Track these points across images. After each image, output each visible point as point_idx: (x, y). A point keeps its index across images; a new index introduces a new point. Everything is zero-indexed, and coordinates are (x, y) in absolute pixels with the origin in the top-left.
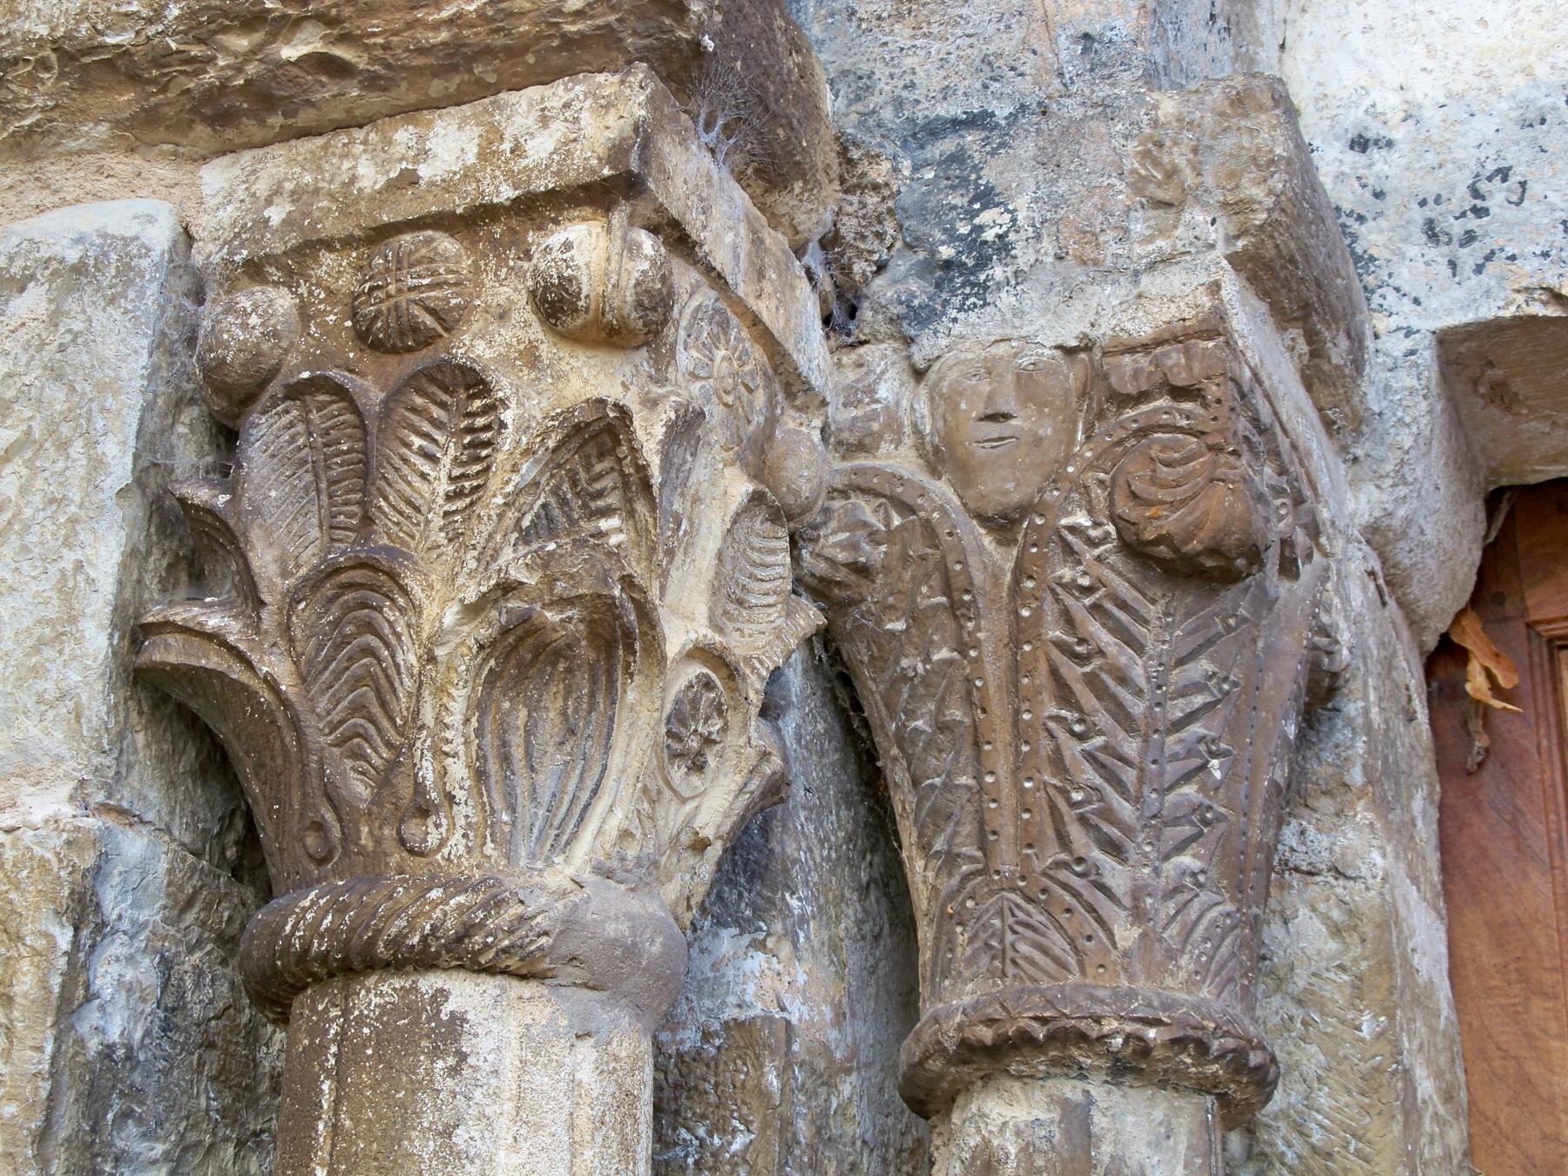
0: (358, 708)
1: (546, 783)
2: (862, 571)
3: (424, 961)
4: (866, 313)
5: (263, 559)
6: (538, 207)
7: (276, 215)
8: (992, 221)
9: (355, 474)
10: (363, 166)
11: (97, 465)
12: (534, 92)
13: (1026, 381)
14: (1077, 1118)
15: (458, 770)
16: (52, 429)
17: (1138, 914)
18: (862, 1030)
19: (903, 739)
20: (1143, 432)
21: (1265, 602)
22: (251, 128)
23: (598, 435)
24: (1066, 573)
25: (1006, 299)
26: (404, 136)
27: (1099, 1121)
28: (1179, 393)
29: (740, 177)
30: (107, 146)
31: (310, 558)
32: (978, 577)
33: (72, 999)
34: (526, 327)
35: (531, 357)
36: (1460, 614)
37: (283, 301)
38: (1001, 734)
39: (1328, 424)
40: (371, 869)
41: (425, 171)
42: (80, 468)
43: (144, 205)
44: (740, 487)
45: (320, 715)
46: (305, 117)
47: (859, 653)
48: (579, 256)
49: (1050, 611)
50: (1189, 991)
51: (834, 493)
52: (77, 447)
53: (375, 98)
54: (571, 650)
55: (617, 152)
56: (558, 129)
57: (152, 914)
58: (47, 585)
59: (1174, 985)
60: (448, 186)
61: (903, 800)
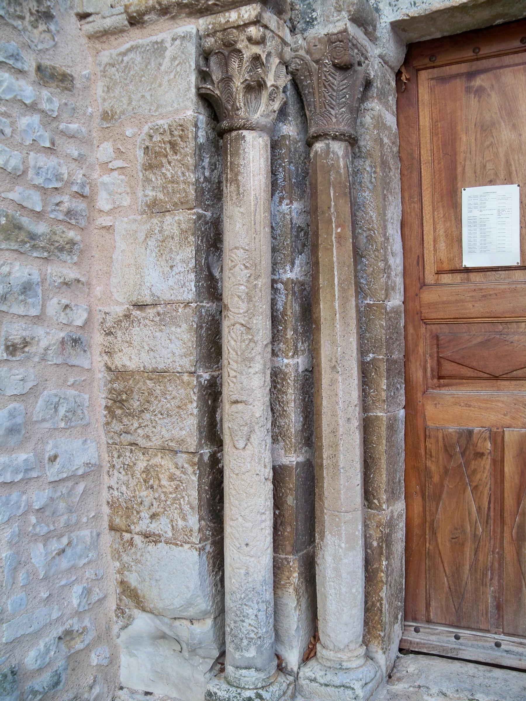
0: (228, 97)
1: (253, 105)
2: (297, 70)
3: (239, 129)
4: (297, 30)
5: (214, 78)
6: (246, 25)
7: (210, 27)
8: (314, 15)
9: (225, 64)
10: (222, 19)
11: (190, 66)
12: (244, 7)
13: (319, 40)
14: (328, 145)
15: (242, 104)
16: (183, 61)
17: (336, 117)
18: (302, 136)
19: (305, 94)
20: (335, 48)
21: (355, 71)
22: (206, 14)
23: (256, 58)
24: (325, 69)
25: (316, 27)
26: (227, 14)
27: (331, 146)
28: (341, 41)
29: (275, 14)
30: (185, 17)
31: (220, 77)
32: (313, 70)
33: (196, 137)
34: (246, 42)
35: (247, 47)
36: (401, 66)
37: (213, 40)
38: (317, 93)
39: (370, 40)
40: (232, 118)
41: (230, 20)
42: (188, 66)
43: (192, 26)
44: (277, 61)
45: (224, 99)
46: (213, 12)
47: (298, 81)
48: (252, 33)
49: (323, 75)
50: (343, 127)
51: (293, 58)
52: (187, 64)
53: (223, 9)
54: (255, 87)
55: (256, 17)
56: (248, 13)
57: (204, 126)
58: (186, 83)
59: (341, 127)
60: (234, 22)
61: (305, 103)
